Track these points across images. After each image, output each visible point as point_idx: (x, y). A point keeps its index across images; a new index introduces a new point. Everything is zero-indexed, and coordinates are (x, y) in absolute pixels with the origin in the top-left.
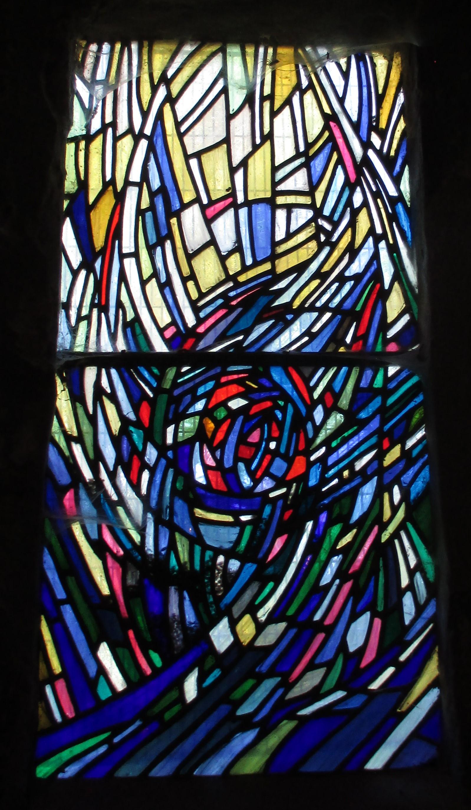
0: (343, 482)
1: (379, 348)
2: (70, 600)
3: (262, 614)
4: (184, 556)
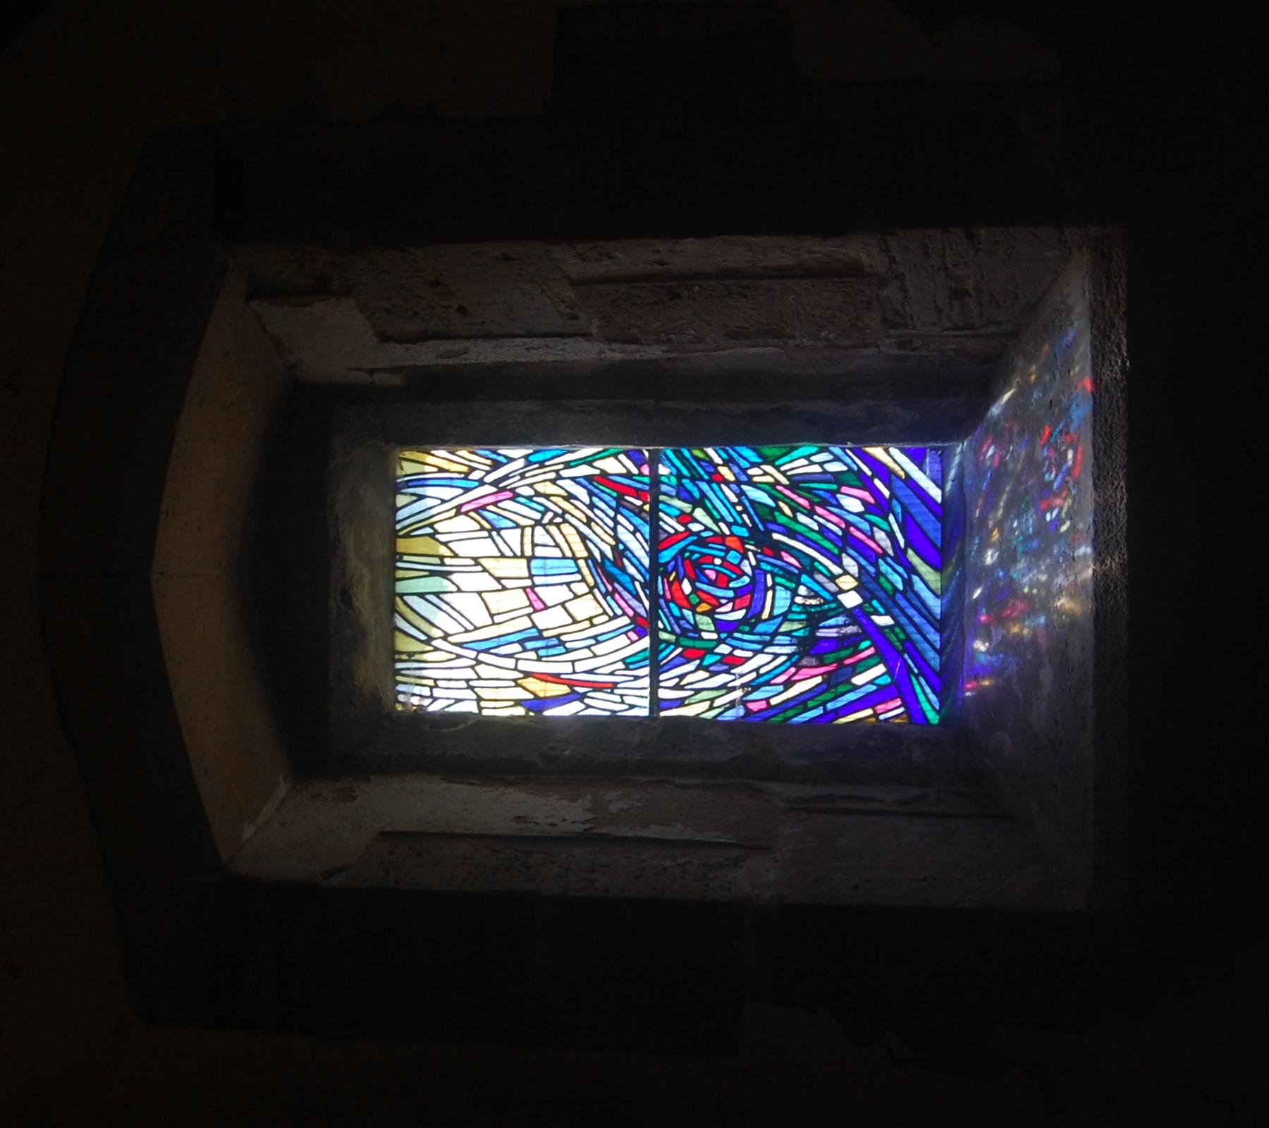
0: (745, 511)
1: (647, 480)
2: (824, 704)
3: (836, 570)
4: (796, 626)
